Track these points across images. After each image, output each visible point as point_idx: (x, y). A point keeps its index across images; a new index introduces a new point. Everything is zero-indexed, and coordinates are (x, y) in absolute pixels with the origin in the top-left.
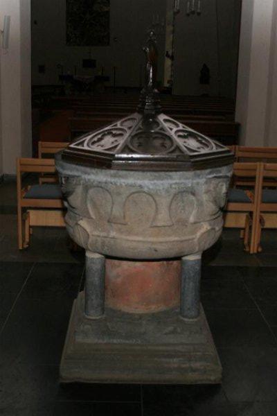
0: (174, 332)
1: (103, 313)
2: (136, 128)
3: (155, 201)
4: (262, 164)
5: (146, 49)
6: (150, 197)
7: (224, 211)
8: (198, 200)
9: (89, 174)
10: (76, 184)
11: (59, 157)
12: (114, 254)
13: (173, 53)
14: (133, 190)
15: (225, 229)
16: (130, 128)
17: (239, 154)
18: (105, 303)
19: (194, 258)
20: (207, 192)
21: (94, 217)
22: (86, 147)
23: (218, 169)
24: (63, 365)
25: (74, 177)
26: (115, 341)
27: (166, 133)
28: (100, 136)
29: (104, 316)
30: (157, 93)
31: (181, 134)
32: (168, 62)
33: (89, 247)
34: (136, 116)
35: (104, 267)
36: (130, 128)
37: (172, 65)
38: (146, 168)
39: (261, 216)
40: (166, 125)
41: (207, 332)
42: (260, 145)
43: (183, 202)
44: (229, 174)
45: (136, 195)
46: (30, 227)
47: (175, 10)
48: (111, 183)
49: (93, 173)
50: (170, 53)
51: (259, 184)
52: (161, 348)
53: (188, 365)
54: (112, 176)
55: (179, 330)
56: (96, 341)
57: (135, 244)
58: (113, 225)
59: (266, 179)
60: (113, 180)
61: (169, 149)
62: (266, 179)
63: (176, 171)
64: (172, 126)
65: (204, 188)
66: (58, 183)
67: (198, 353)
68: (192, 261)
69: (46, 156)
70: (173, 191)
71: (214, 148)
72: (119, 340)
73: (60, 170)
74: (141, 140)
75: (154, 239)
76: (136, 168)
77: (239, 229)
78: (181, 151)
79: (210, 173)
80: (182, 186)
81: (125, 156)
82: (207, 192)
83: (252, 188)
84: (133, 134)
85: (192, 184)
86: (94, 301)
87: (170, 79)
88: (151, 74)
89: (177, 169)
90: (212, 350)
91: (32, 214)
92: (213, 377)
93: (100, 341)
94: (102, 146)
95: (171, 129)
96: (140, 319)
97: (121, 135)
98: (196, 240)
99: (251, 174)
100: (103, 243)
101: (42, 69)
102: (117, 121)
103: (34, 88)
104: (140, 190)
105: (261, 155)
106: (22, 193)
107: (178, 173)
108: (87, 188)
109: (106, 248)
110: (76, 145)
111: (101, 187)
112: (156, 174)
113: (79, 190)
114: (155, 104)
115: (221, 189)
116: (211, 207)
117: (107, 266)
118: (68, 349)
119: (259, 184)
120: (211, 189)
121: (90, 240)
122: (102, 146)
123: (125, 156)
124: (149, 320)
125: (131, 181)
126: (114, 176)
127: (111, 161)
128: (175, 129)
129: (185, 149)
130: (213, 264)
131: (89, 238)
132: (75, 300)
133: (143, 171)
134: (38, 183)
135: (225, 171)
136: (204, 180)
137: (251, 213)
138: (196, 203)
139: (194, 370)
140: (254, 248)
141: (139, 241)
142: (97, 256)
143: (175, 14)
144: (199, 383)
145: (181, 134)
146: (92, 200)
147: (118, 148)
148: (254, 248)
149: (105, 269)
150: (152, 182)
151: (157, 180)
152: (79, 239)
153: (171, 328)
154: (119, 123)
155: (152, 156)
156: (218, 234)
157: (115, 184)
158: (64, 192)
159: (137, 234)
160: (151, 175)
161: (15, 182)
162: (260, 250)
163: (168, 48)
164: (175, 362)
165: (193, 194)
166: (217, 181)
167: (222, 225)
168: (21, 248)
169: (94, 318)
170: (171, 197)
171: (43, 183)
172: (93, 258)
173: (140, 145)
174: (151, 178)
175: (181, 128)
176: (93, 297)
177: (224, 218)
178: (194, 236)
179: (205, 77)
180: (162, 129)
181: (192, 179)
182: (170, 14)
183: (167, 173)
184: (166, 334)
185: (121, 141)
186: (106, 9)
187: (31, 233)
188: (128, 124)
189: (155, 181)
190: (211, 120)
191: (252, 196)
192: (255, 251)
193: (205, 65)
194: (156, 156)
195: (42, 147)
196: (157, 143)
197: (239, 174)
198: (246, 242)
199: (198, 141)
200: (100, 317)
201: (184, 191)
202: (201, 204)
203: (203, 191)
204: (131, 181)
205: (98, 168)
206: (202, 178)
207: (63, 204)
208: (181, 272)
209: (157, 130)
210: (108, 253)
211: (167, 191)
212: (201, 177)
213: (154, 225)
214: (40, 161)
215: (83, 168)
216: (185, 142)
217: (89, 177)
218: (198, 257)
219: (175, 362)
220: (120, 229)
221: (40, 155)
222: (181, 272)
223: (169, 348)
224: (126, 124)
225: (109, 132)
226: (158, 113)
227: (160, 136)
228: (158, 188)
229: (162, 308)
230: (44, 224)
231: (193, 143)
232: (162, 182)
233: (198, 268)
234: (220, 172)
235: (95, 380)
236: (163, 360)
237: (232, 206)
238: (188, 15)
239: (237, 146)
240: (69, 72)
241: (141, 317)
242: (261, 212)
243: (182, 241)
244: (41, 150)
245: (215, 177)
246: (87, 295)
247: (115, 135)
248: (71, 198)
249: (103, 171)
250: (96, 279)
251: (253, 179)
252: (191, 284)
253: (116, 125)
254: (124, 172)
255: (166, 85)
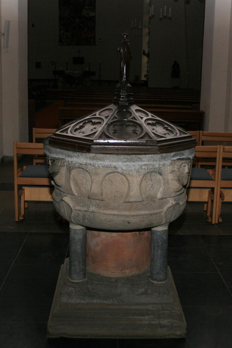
0: (145, 293)
1: (85, 277)
2: (112, 118)
3: (128, 180)
4: (222, 146)
5: (120, 50)
6: (124, 177)
7: (187, 188)
8: (164, 179)
9: (72, 157)
10: (61, 166)
11: (47, 142)
12: (93, 226)
13: (148, 52)
14: (109, 171)
15: (188, 202)
16: (106, 117)
17: (204, 138)
18: (87, 268)
19: (162, 229)
20: (172, 172)
21: (76, 194)
22: (69, 134)
23: (181, 152)
24: (50, 323)
25: (58, 159)
26: (95, 301)
27: (138, 122)
28: (81, 124)
29: (86, 279)
30: (130, 87)
31: (150, 122)
32: (145, 59)
33: (73, 220)
34: (112, 106)
35: (85, 237)
36: (106, 117)
37: (148, 62)
38: (120, 152)
39: (221, 191)
40: (138, 114)
41: (174, 292)
42: (222, 131)
43: (152, 181)
44: (191, 157)
45: (111, 175)
46: (25, 202)
47: (150, 15)
48: (91, 165)
49: (75, 157)
50: (146, 52)
51: (219, 164)
52: (133, 307)
53: (157, 322)
54: (90, 159)
55: (149, 291)
56: (78, 301)
57: (111, 217)
58: (92, 201)
59: (225, 160)
60: (92, 162)
61: (140, 135)
62: (225, 160)
63: (145, 154)
64: (142, 115)
65: (169, 169)
66: (46, 164)
67: (166, 312)
68: (160, 231)
69: (39, 140)
70: (143, 172)
71: (178, 134)
72: (98, 301)
73: (48, 153)
74: (117, 128)
75: (127, 213)
76: (111, 152)
77: (203, 203)
78: (150, 137)
79: (174, 156)
80: (151, 167)
81: (102, 141)
82: (172, 172)
83: (213, 167)
84: (109, 123)
85: (159, 165)
86: (77, 266)
87: (146, 73)
88: (125, 71)
89: (146, 152)
90: (178, 309)
91: (27, 190)
92: (179, 332)
93: (82, 301)
94: (83, 133)
95: (142, 118)
96: (116, 281)
97: (100, 123)
98: (163, 213)
99: (212, 155)
100: (84, 216)
101: (38, 65)
102: (96, 110)
103: (30, 81)
104: (115, 171)
105: (221, 139)
106: (18, 172)
107: (147, 156)
108: (70, 169)
109: (87, 220)
110: (60, 132)
111: (82, 168)
112: (129, 157)
113: (63, 171)
114: (128, 96)
115: (184, 169)
116: (175, 185)
117: (87, 235)
118: (55, 309)
119: (219, 164)
120: (176, 169)
121: (73, 213)
122: (83, 133)
123: (102, 141)
124: (123, 283)
125: (107, 163)
126: (93, 159)
127: (90, 145)
128: (145, 118)
129: (153, 135)
130: (180, 233)
131: (72, 212)
132: (62, 265)
133: (118, 154)
134: (32, 164)
135: (188, 154)
136: (170, 161)
137: (213, 189)
138: (162, 181)
139: (162, 326)
140: (215, 219)
141: (114, 215)
142: (79, 227)
143: (150, 18)
144: (167, 337)
145: (150, 122)
146: (74, 179)
147: (96, 134)
148: (215, 219)
149: (86, 239)
150: (126, 164)
151: (129, 162)
152: (64, 212)
153: (143, 290)
154: (97, 113)
155: (125, 142)
156: (182, 208)
157: (94, 166)
158: (51, 172)
159: (112, 209)
160: (124, 158)
161: (12, 162)
162: (221, 220)
163: (145, 48)
164: (146, 320)
165: (161, 174)
166: (179, 163)
167: (185, 201)
168: (17, 220)
169: (77, 281)
170: (141, 176)
171: (37, 164)
172: (75, 229)
173: (115, 132)
174: (124, 160)
175: (150, 117)
176: (76, 263)
177: (188, 194)
178: (161, 210)
179: (176, 71)
180: (134, 118)
181: (160, 161)
182: (146, 18)
183: (138, 156)
184: (138, 295)
185: (99, 129)
186: (92, 14)
187: (26, 207)
188: (106, 113)
189: (128, 163)
190: (167, 108)
191: (214, 175)
192: (217, 222)
193: (175, 62)
194: (128, 141)
195: (36, 133)
196: (130, 129)
197: (199, 155)
198: (208, 214)
199: (165, 128)
200: (82, 280)
201: (152, 172)
202: (166, 182)
203: (169, 172)
204: (107, 163)
205: (79, 152)
206: (168, 160)
207: (50, 183)
208: (151, 241)
209: (130, 118)
210: (88, 225)
211: (138, 172)
212: (166, 159)
213: (127, 200)
214: (34, 145)
215: (66, 152)
216: (153, 129)
217: (72, 160)
218: (165, 228)
219: (146, 320)
220: (98, 205)
221: (34, 140)
222: (151, 241)
223: (141, 307)
224: (103, 113)
225: (90, 121)
226: (131, 104)
227: (131, 124)
228: (130, 169)
229: (135, 272)
230: (37, 200)
231: (160, 130)
232: (133, 164)
233: (165, 237)
234: (183, 154)
235: (73, 336)
236: (136, 317)
237: (194, 183)
238: (161, 19)
239: (201, 131)
240: (61, 69)
241: (117, 280)
242: (222, 188)
243: (151, 215)
244: (35, 136)
245: (179, 159)
246: (70, 262)
247: (94, 124)
248: (56, 178)
249: (84, 154)
250: (79, 247)
251: (214, 159)
252: (159, 251)
253: (95, 115)
254: (101, 155)
255: (143, 79)
